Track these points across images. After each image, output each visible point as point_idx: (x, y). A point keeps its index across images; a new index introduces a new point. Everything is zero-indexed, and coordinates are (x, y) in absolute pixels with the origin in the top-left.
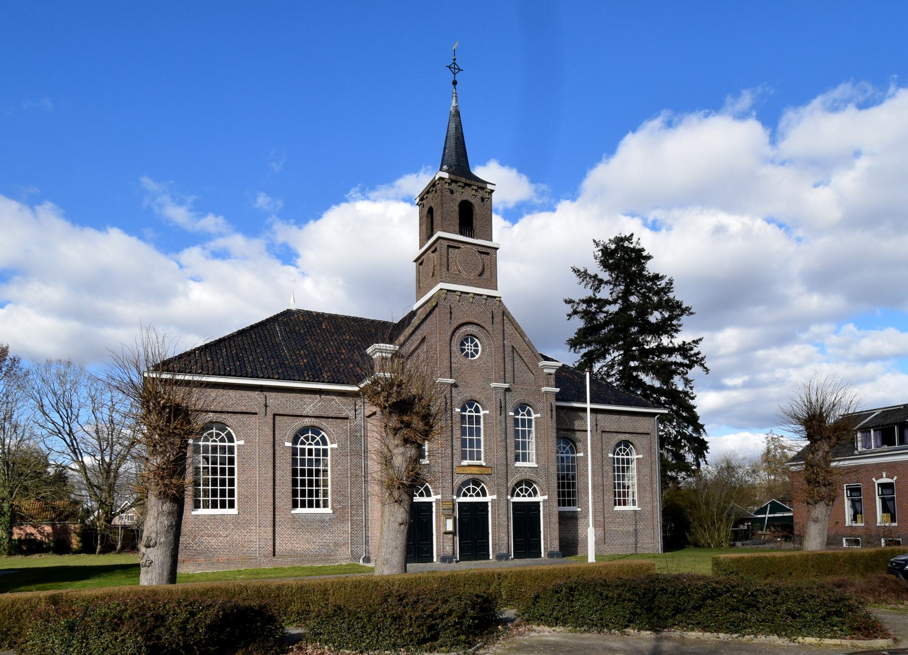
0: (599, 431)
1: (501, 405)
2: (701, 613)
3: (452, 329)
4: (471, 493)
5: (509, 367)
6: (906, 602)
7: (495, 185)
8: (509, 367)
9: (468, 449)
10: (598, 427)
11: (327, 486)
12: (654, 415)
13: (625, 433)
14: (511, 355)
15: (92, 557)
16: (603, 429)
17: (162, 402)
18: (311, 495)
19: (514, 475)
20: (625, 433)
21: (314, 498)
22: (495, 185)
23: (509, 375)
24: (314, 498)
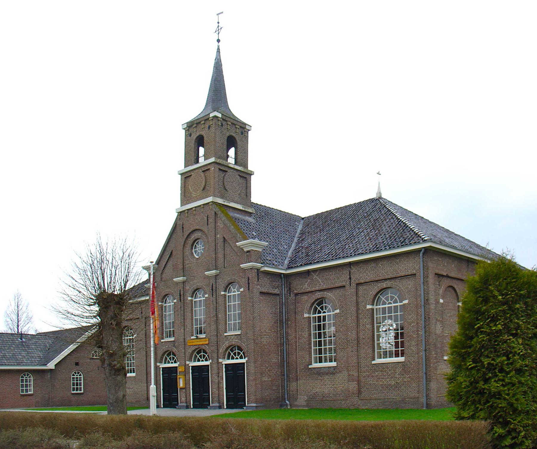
0: (354, 285)
1: (180, 293)
2: (475, 378)
3: (184, 240)
4: (237, 357)
5: (220, 256)
6: (461, 448)
7: (222, 13)
8: (220, 256)
9: (399, 313)
10: (352, 281)
11: (81, 381)
12: (418, 251)
13: (386, 280)
14: (222, 245)
15: (380, 360)
16: (357, 282)
17: (349, 322)
18: (77, 385)
19: (224, 343)
20: (386, 280)
21: (79, 387)
22: (222, 13)
23: (220, 261)
24: (79, 387)
